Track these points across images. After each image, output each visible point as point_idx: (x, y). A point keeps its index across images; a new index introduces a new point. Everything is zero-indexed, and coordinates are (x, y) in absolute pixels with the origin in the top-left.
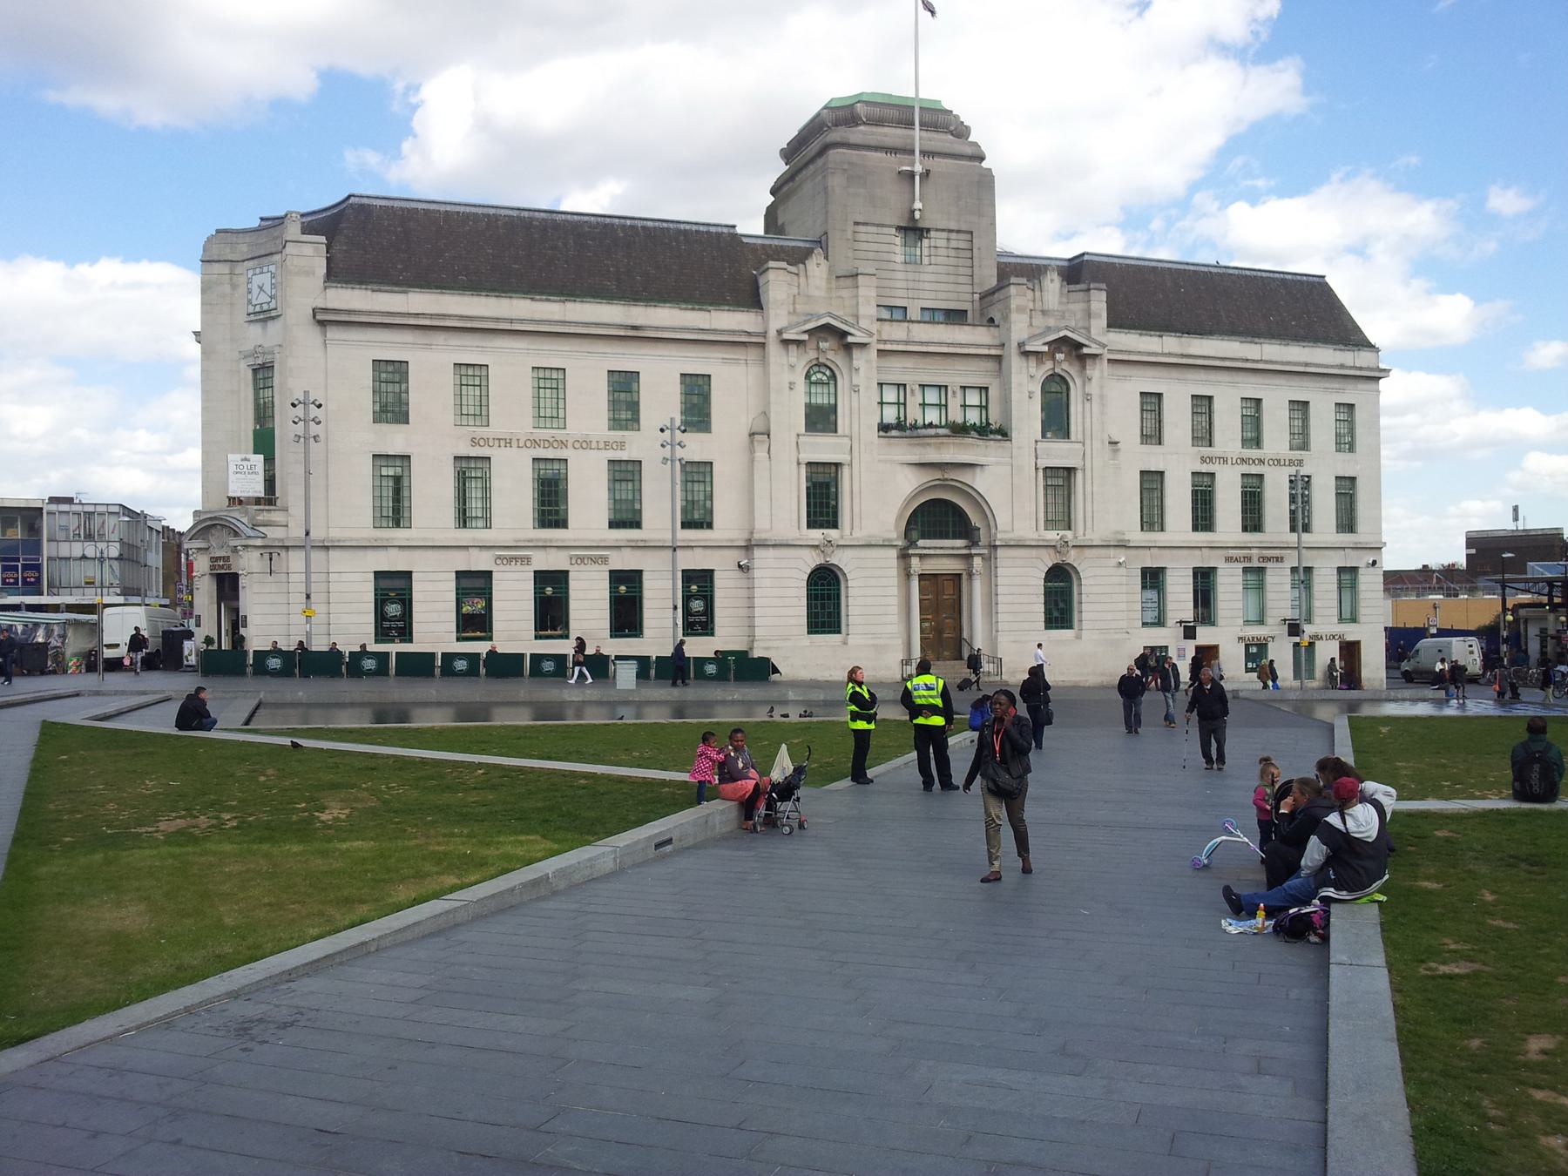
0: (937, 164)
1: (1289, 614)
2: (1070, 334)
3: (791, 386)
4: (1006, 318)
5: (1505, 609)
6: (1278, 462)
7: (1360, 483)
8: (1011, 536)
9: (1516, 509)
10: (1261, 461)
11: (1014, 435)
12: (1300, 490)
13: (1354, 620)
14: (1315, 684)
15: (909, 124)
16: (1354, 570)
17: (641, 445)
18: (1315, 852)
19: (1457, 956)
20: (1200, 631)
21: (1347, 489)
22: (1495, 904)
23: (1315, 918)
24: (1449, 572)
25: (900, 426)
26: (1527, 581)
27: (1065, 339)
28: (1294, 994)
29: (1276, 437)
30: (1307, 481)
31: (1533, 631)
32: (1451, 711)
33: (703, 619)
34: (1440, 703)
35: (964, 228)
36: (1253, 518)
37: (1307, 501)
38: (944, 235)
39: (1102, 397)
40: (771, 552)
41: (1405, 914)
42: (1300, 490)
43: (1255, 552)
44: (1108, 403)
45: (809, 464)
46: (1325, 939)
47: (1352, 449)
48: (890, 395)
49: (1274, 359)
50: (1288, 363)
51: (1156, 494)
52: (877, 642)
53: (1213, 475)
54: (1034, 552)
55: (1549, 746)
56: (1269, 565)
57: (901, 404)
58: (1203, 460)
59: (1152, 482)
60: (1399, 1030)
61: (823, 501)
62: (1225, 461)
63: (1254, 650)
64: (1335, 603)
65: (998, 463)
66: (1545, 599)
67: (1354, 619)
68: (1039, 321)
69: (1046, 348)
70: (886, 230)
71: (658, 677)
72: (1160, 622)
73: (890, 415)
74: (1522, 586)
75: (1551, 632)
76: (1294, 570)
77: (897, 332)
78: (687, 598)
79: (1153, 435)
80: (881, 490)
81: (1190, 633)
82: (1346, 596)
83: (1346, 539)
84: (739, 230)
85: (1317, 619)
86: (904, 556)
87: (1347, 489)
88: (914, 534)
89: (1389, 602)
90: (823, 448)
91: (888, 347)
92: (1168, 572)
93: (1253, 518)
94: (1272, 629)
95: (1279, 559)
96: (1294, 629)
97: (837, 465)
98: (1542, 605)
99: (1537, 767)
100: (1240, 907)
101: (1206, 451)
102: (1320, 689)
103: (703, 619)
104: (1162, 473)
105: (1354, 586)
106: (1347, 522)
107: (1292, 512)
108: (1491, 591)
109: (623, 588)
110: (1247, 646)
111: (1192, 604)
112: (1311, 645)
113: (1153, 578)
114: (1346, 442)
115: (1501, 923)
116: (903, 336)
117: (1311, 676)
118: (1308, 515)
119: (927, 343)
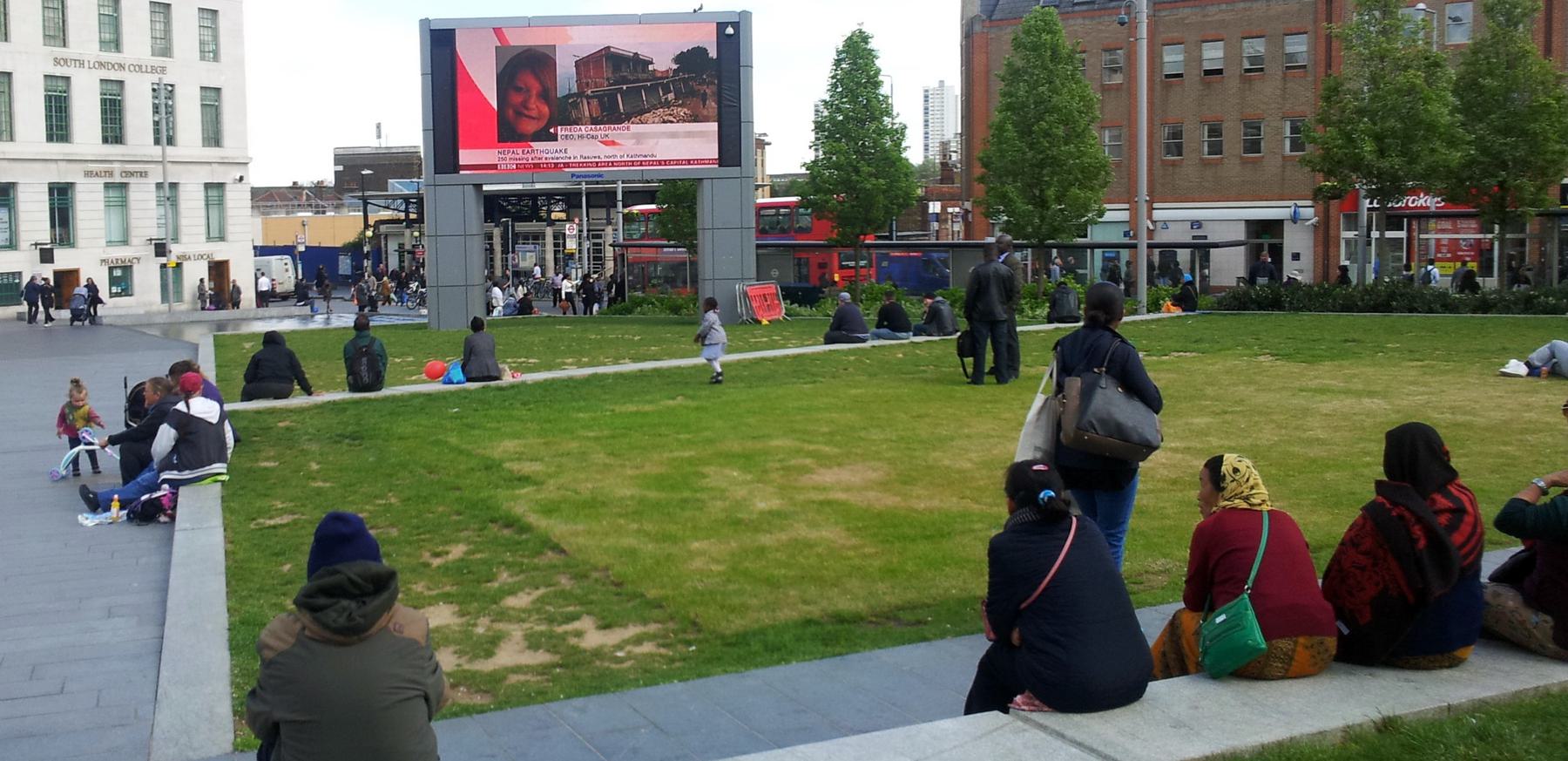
1: (156, 233)
5: (367, 226)
6: (139, 68)
7: (225, 94)
9: (378, 126)
10: (121, 67)
12: (164, 101)
13: (222, 238)
14: (183, 307)
16: (221, 186)
18: (165, 437)
19: (284, 511)
20: (59, 253)
21: (212, 100)
22: (318, 472)
23: (164, 501)
24: (318, 189)
26: (386, 197)
28: (143, 560)
30: (171, 91)
31: (392, 246)
32: (318, 322)
34: (304, 318)
36: (113, 131)
37: (170, 111)
41: (242, 488)
42: (164, 101)
43: (116, 165)
46: (173, 518)
47: (216, 58)
53: (67, 79)
55: (373, 340)
58: (57, 61)
60: (227, 568)
62: (82, 64)
63: (118, 273)
64: (203, 221)
66: (402, 216)
67: (222, 238)
72: (12, 245)
74: (382, 202)
75: (408, 247)
76: (159, 186)
81: (47, 256)
82: (214, 213)
83: (212, 153)
85: (184, 238)
87: (212, 100)
89: (258, 220)
92: (20, 189)
93: (113, 131)
94: (138, 249)
95: (143, 174)
96: (161, 250)
98: (398, 221)
99: (364, 360)
100: (96, 504)
101: (60, 51)
102: (188, 312)
104: (9, 74)
105: (221, 202)
106: (213, 136)
107: (156, 123)
108: (352, 207)
110: (111, 269)
112: (179, 265)
114: (210, 50)
115: (320, 484)
117: (180, 299)
118: (172, 127)
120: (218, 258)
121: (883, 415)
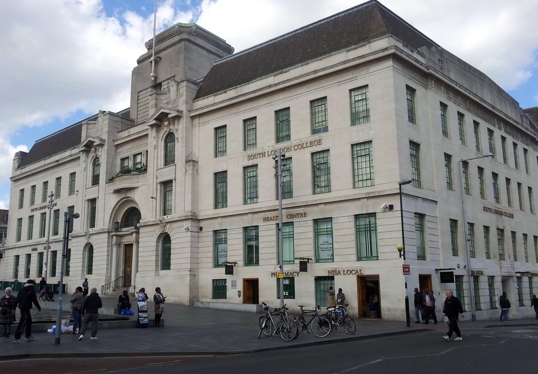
29: (300, 128)
51: (446, 56)
52: (98, 277)
56: (294, 220)
58: (250, 157)
63: (287, 282)
65: (142, 185)
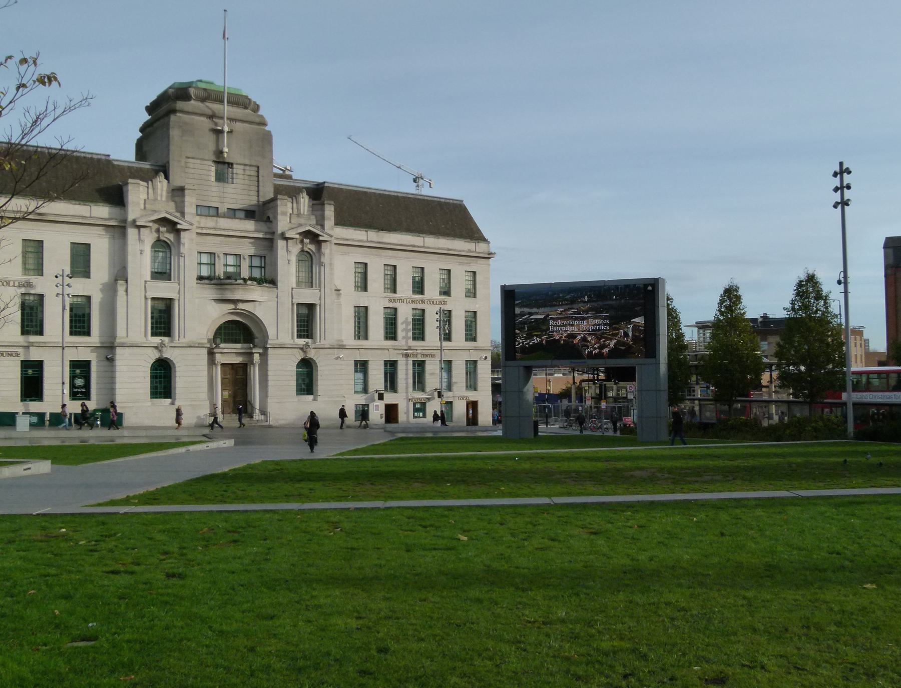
0: (239, 126)
2: (312, 229)
3: (142, 252)
4: (276, 218)
8: (276, 342)
10: (423, 302)
11: (279, 284)
12: (447, 317)
15: (222, 102)
17: (44, 285)
25: (209, 278)
27: (309, 232)
29: (432, 289)
33: (84, 390)
35: (254, 164)
38: (242, 167)
39: (331, 264)
40: (127, 350)
44: (339, 266)
45: (153, 299)
48: (205, 259)
49: (408, 243)
50: (438, 249)
54: (290, 351)
57: (212, 265)
58: (390, 301)
59: (362, 314)
61: (163, 320)
63: (418, 406)
68: (295, 220)
69: (298, 236)
70: (206, 162)
71: (102, 425)
73: (205, 272)
77: (209, 222)
78: (73, 378)
79: (363, 285)
80: (200, 315)
84: (112, 157)
85: (454, 388)
86: (211, 354)
88: (218, 341)
90: (163, 289)
91: (204, 231)
95: (432, 356)
97: (170, 299)
103: (84, 390)
109: (30, 372)
110: (414, 404)
111: (383, 381)
113: (362, 366)
116: (365, 239)
119: (228, 230)
120: (472, 399)
121: (780, 548)
